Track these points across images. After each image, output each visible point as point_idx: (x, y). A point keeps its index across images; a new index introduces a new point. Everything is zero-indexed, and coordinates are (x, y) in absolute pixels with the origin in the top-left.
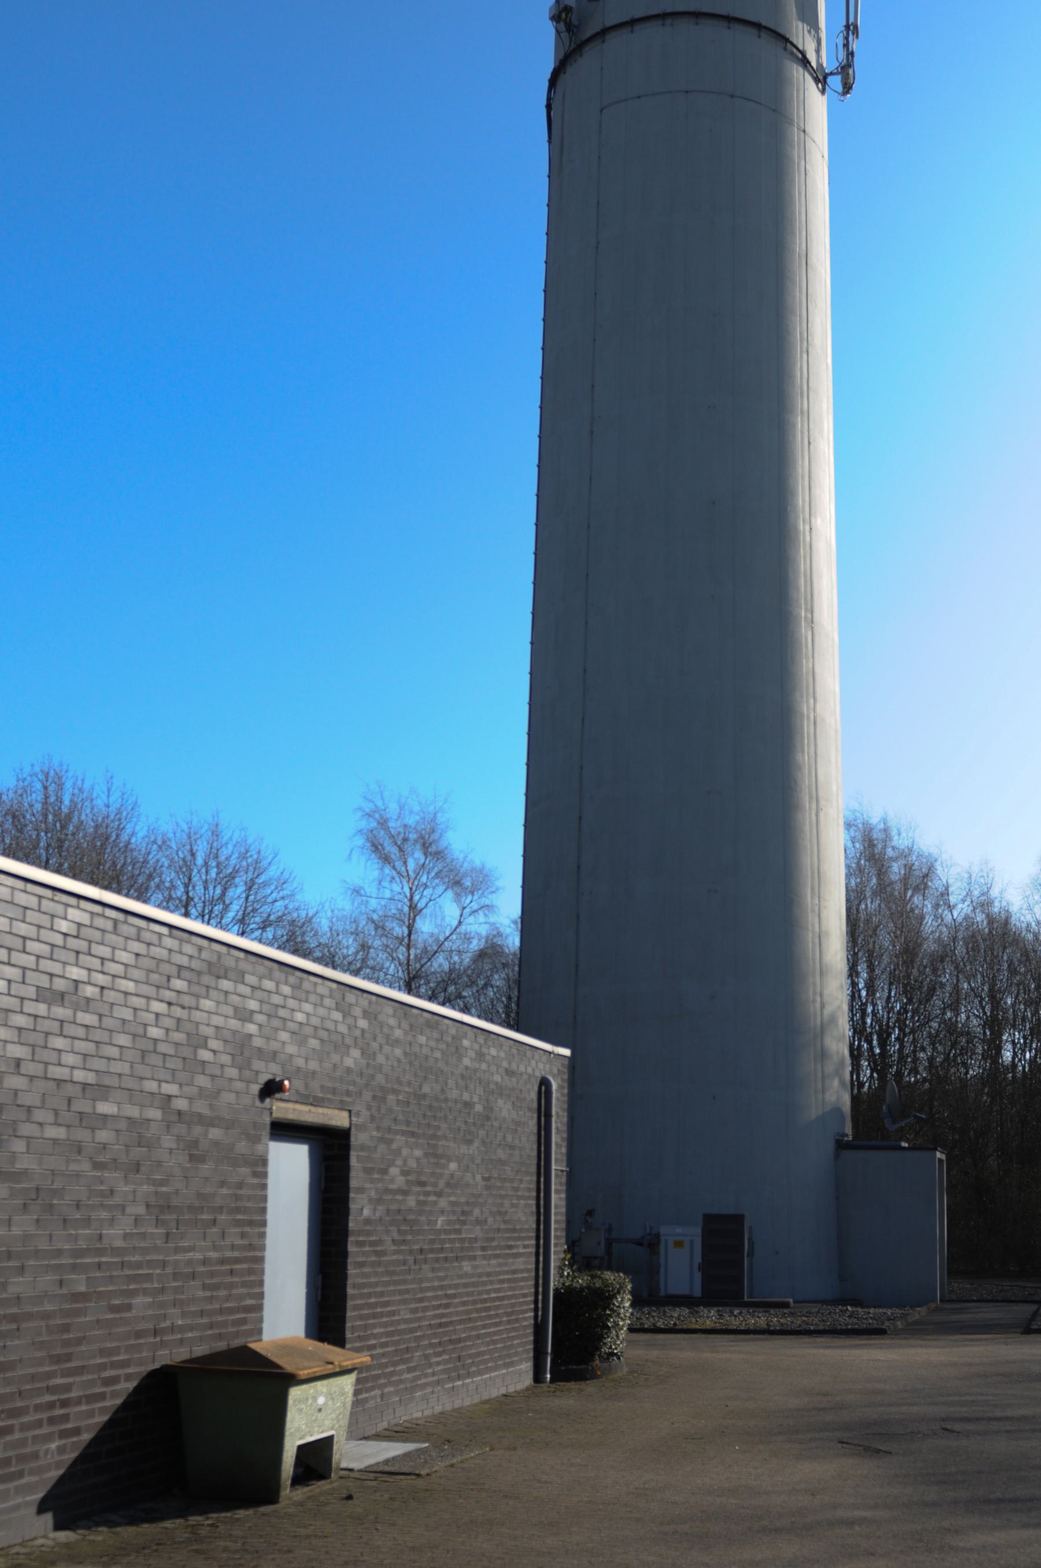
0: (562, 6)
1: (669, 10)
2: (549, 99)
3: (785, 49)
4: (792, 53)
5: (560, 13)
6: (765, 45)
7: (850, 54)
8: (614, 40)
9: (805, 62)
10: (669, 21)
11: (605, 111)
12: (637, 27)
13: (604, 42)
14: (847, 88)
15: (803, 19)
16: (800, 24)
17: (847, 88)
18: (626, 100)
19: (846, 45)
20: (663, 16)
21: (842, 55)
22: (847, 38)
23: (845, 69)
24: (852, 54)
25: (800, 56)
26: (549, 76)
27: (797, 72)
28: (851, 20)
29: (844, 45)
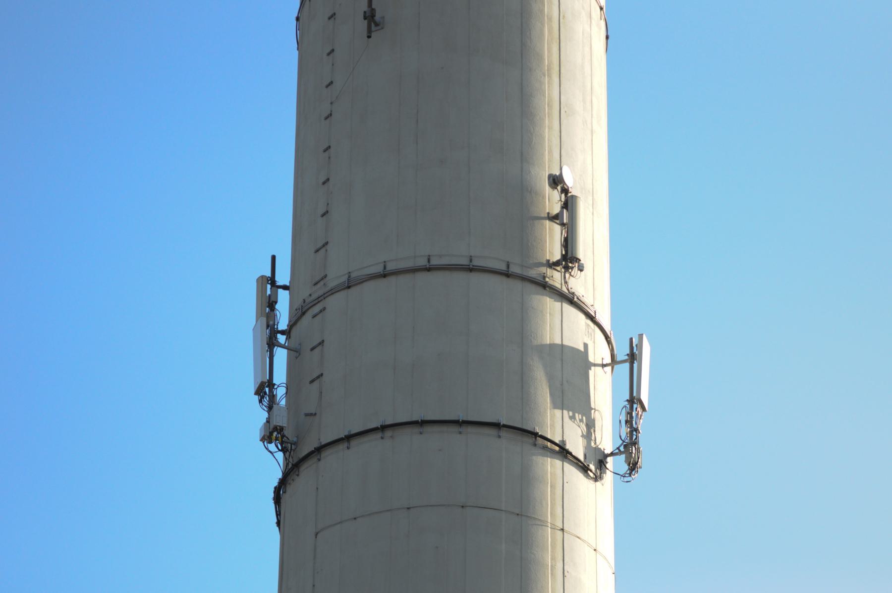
0: (272, 427)
1: (388, 422)
2: (278, 514)
3: (535, 445)
4: (545, 448)
5: (271, 433)
6: (506, 447)
7: (634, 430)
8: (330, 458)
9: (564, 453)
10: (388, 433)
11: (319, 535)
12: (354, 442)
13: (319, 460)
14: (633, 467)
15: (560, 403)
16: (558, 413)
17: (633, 467)
18: (341, 522)
19: (629, 422)
20: (384, 428)
21: (625, 430)
22: (630, 414)
23: (629, 446)
24: (636, 430)
25: (557, 448)
26: (272, 495)
27: (552, 466)
28: (635, 394)
29: (626, 422)
